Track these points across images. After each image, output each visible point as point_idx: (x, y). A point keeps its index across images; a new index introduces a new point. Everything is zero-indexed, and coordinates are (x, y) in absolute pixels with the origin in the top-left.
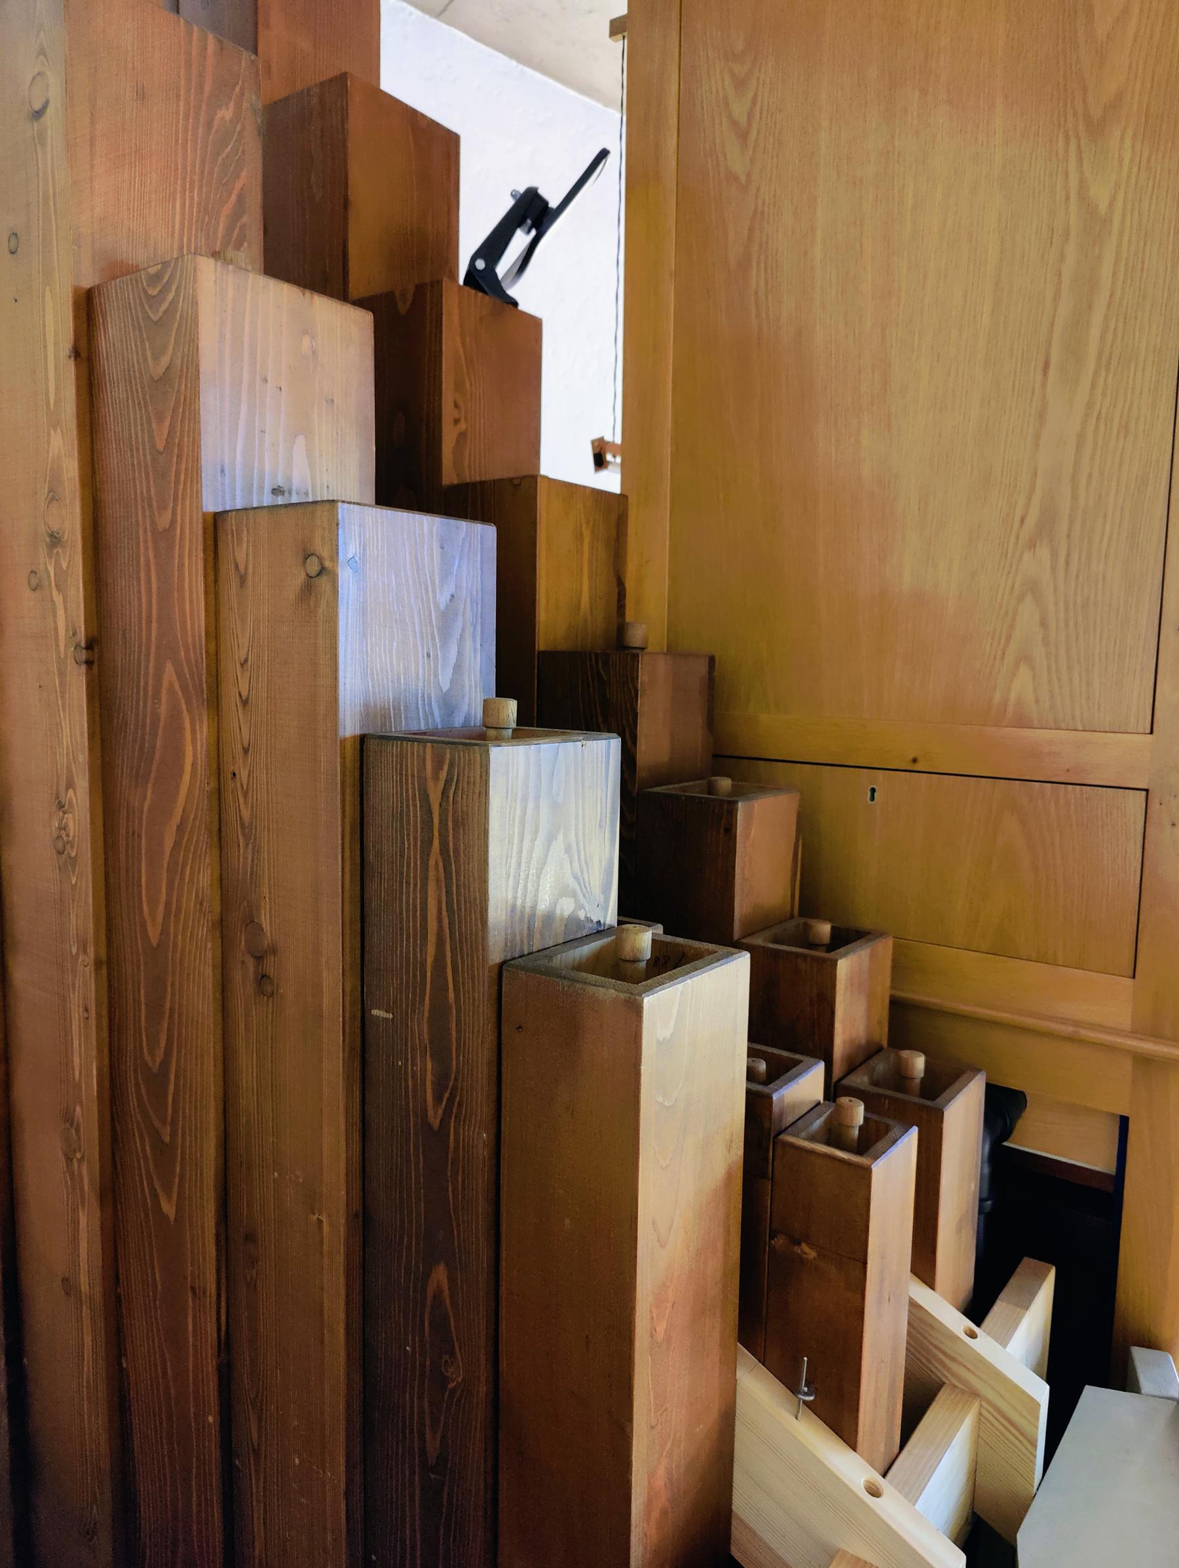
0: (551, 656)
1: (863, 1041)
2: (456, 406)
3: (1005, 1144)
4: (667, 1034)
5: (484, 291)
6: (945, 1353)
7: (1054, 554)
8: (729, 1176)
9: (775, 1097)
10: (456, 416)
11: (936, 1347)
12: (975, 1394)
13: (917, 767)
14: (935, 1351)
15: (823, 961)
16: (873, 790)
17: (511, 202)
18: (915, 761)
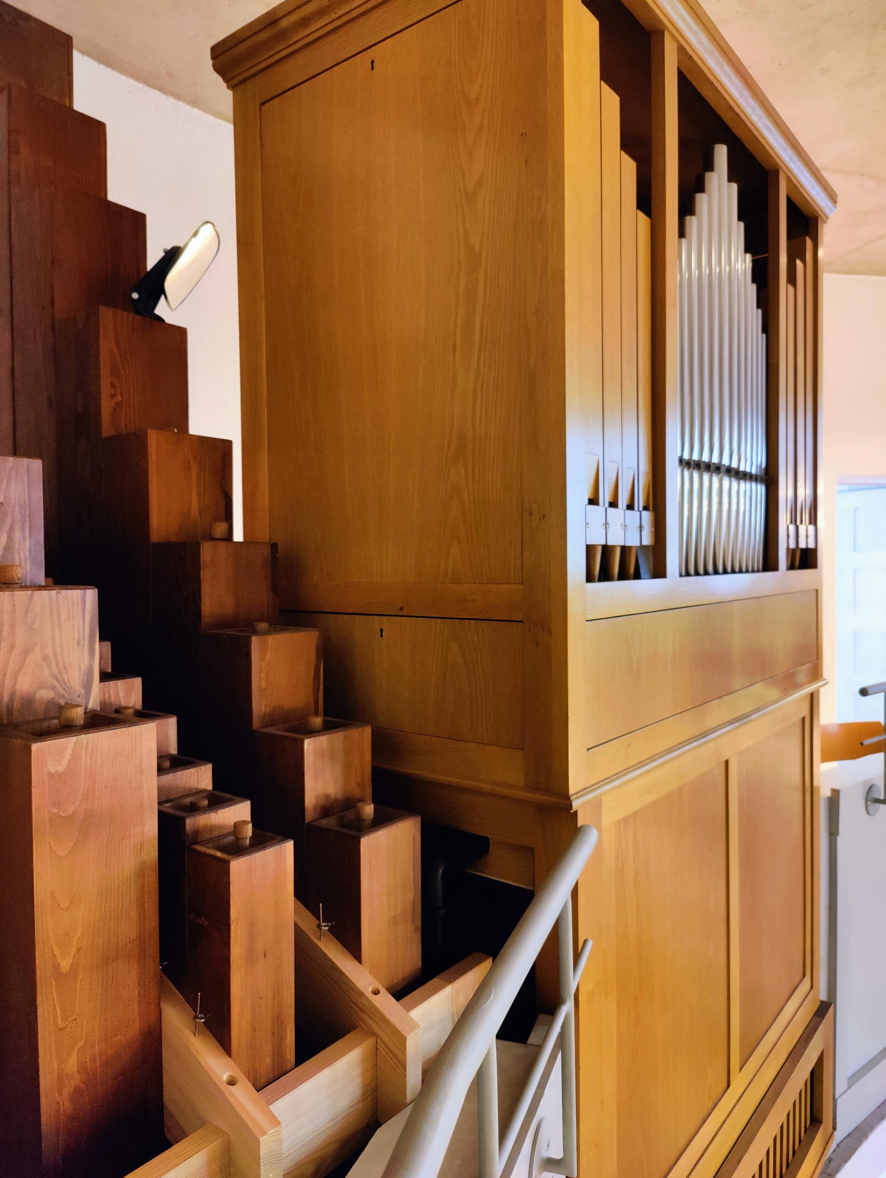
0: (157, 545)
1: (333, 796)
2: (112, 385)
3: (467, 870)
4: (61, 769)
5: (141, 314)
6: (358, 1006)
7: (466, 467)
8: (141, 872)
9: (188, 821)
10: (113, 392)
11: (353, 1002)
12: (374, 1034)
13: (404, 612)
14: (355, 1008)
15: (297, 740)
16: (382, 630)
17: (163, 254)
18: (402, 609)
